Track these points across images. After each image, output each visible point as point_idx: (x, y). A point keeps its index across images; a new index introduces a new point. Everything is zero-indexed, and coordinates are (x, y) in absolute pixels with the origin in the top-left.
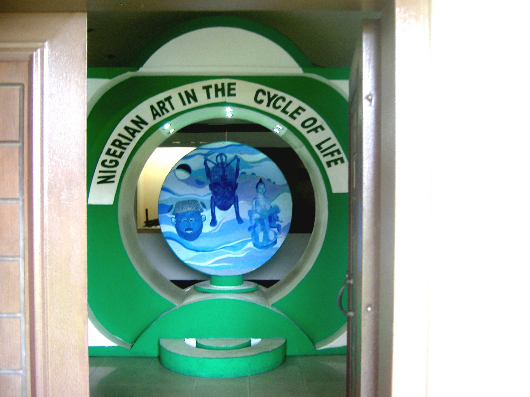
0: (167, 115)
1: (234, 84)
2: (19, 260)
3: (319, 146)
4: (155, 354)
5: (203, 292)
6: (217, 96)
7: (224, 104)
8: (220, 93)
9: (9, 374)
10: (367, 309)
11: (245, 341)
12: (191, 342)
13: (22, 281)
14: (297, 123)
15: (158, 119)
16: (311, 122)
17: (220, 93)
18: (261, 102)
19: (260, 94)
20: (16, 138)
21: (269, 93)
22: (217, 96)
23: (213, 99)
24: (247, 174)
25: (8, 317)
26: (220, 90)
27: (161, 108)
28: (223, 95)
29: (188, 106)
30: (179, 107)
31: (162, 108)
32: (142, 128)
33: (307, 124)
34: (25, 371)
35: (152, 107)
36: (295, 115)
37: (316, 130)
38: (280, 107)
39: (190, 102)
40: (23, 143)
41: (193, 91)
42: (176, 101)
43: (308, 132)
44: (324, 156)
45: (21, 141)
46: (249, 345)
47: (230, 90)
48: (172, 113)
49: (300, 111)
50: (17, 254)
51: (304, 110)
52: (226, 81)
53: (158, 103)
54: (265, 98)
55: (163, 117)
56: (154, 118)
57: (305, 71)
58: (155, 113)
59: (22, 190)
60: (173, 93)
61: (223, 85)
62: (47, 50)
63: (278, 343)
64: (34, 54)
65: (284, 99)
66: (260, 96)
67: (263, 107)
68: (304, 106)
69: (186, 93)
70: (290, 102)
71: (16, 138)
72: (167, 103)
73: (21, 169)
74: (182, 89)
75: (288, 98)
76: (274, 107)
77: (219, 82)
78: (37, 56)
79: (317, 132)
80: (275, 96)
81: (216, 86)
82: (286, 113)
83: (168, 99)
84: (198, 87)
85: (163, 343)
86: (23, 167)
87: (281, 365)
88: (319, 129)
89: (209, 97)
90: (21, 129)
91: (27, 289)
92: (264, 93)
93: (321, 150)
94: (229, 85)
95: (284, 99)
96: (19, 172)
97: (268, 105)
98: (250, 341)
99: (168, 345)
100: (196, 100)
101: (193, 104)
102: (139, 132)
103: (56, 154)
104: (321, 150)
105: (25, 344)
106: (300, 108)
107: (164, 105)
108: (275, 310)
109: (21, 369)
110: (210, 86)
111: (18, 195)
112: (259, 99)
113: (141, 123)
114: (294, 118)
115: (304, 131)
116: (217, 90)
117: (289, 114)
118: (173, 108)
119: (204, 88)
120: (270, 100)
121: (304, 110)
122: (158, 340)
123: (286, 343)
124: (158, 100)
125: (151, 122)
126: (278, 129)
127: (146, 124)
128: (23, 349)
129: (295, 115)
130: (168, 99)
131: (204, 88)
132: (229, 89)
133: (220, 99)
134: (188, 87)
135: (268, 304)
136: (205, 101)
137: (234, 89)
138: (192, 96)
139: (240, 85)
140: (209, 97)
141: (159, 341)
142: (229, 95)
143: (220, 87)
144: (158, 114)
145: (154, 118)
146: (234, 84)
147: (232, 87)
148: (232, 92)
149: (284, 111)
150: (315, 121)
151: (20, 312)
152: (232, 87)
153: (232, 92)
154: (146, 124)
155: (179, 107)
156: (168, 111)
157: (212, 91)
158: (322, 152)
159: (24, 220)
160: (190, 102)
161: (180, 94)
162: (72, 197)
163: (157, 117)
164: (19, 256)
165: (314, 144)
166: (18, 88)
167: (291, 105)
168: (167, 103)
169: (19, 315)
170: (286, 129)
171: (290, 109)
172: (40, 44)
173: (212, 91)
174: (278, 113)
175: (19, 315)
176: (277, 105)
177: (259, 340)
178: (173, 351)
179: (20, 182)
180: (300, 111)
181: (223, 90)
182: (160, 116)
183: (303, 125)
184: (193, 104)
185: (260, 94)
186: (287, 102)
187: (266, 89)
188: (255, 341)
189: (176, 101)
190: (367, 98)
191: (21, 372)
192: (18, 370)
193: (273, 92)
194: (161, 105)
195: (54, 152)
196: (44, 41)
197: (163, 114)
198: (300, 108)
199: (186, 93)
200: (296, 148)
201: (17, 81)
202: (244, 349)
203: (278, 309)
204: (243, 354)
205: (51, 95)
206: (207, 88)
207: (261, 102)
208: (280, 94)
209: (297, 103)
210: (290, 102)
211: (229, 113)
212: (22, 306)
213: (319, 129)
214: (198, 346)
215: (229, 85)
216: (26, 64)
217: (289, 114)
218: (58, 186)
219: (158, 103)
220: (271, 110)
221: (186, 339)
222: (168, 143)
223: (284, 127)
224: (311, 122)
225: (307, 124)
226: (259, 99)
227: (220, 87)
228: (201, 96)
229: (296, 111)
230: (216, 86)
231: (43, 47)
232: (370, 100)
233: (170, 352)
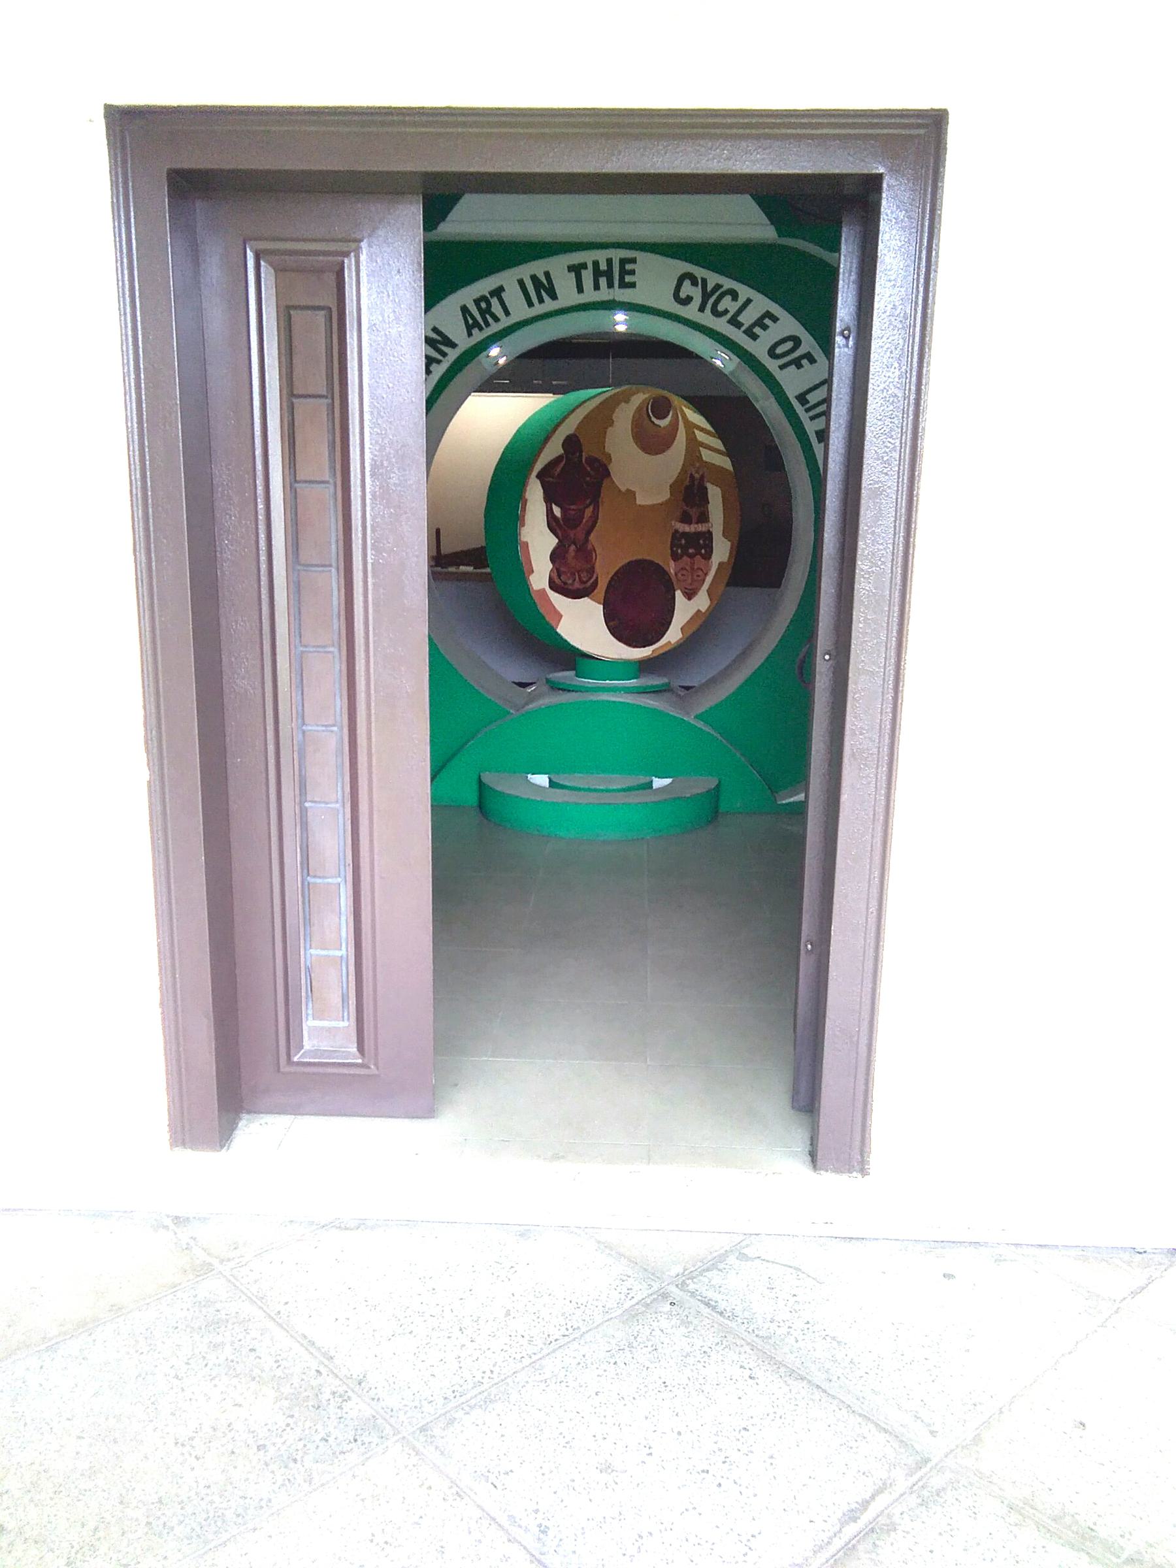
0: (495, 328)
1: (633, 261)
2: (330, 571)
3: (802, 398)
4: (472, 798)
5: (563, 690)
6: (597, 287)
7: (611, 306)
8: (603, 281)
9: (318, 731)
10: (825, 660)
11: (643, 779)
12: (542, 780)
13: (335, 603)
14: (759, 349)
15: (478, 336)
16: (789, 345)
17: (603, 281)
18: (688, 300)
19: (687, 283)
20: (323, 391)
21: (704, 281)
22: (597, 287)
23: (590, 295)
24: (484, 544)
25: (315, 652)
26: (602, 274)
27: (483, 313)
28: (610, 285)
29: (539, 309)
30: (520, 310)
31: (486, 312)
32: (444, 355)
33: (779, 351)
34: (341, 729)
35: (465, 310)
36: (757, 330)
37: (797, 363)
38: (726, 311)
39: (541, 301)
40: (333, 399)
41: (547, 274)
42: (513, 296)
43: (782, 367)
44: (812, 418)
45: (329, 396)
46: (650, 785)
47: (624, 276)
48: (505, 322)
49: (767, 321)
50: (327, 563)
51: (775, 319)
52: (617, 255)
53: (477, 302)
54: (696, 293)
55: (488, 332)
56: (470, 334)
57: (780, 234)
58: (471, 322)
59: (333, 468)
60: (508, 279)
61: (609, 262)
62: (363, 257)
63: (703, 783)
64: (346, 261)
65: (734, 295)
66: (687, 289)
67: (690, 312)
68: (776, 309)
69: (534, 278)
70: (749, 301)
71: (323, 391)
72: (494, 301)
73: (331, 438)
74: (525, 271)
75: (744, 292)
76: (716, 313)
77: (601, 256)
78: (350, 264)
79: (799, 366)
80: (718, 287)
81: (596, 264)
82: (738, 325)
83: (498, 292)
84: (557, 267)
85: (487, 778)
86: (334, 433)
87: (710, 822)
88: (805, 362)
89: (580, 289)
90: (330, 377)
91: (343, 613)
92: (694, 283)
93: (808, 406)
94: (623, 262)
95: (734, 295)
96: (329, 443)
97: (702, 309)
98: (652, 782)
99: (499, 783)
100: (554, 297)
101: (549, 305)
102: (439, 362)
103: (382, 417)
104: (808, 406)
105: (341, 689)
106: (768, 315)
107: (489, 305)
108: (700, 724)
109: (334, 725)
110: (584, 266)
111: (327, 477)
112: (683, 295)
113: (438, 342)
114: (754, 337)
115: (772, 365)
116: (597, 273)
117: (743, 328)
118: (507, 313)
119: (571, 268)
120: (706, 296)
121: (775, 319)
122: (476, 777)
123: (718, 786)
124: (477, 295)
125: (464, 342)
126: (722, 360)
127: (453, 345)
128: (338, 698)
129: (757, 330)
130: (498, 292)
131: (571, 268)
132: (623, 272)
133: (604, 294)
134: (537, 268)
135: (688, 714)
136: (574, 298)
137: (632, 272)
138: (545, 287)
139: (647, 265)
140: (580, 289)
141: (480, 776)
142: (624, 285)
143: (603, 267)
144: (476, 324)
145: (470, 334)
146: (633, 261)
147: (628, 267)
148: (628, 279)
149: (734, 322)
150: (797, 341)
151: (333, 646)
152: (628, 267)
153: (628, 279)
154: (453, 345)
155: (520, 310)
156: (497, 319)
157: (587, 276)
158: (807, 410)
159: (336, 511)
160: (541, 301)
161: (521, 283)
162: (406, 481)
163: (475, 331)
164: (330, 566)
165: (791, 394)
166: (323, 312)
167: (750, 307)
168: (494, 301)
169: (331, 649)
170: (736, 360)
171: (746, 319)
172: (353, 245)
173: (587, 276)
174: (721, 325)
175: (331, 649)
176: (721, 308)
177: (668, 781)
178: (512, 792)
179: (329, 457)
180: (767, 321)
181: (609, 273)
182: (481, 329)
183: (772, 353)
184: (549, 305)
185: (687, 283)
186: (742, 300)
187: (699, 272)
188: (658, 783)
189: (513, 296)
190: (842, 334)
191: (335, 729)
192: (332, 726)
193: (713, 279)
194: (483, 305)
195: (379, 414)
196: (361, 241)
197: (487, 324)
198: (768, 315)
199: (534, 278)
200: (757, 401)
201: (317, 302)
202: (641, 791)
203: (706, 722)
204: (637, 800)
205: (372, 326)
206: (577, 269)
207: (688, 300)
208: (728, 283)
209: (761, 304)
210: (749, 301)
211: (621, 322)
212: (336, 637)
213: (805, 362)
214: (552, 783)
215: (623, 262)
216: (333, 277)
217: (743, 328)
218: (385, 464)
219: (477, 302)
220: (707, 319)
221: (529, 776)
222: (493, 384)
223: (734, 357)
224: (789, 345)
225: (779, 351)
226: (683, 295)
227: (603, 267)
228: (567, 293)
229: (760, 323)
230: (596, 264)
231: (357, 251)
232: (847, 338)
233: (502, 794)
